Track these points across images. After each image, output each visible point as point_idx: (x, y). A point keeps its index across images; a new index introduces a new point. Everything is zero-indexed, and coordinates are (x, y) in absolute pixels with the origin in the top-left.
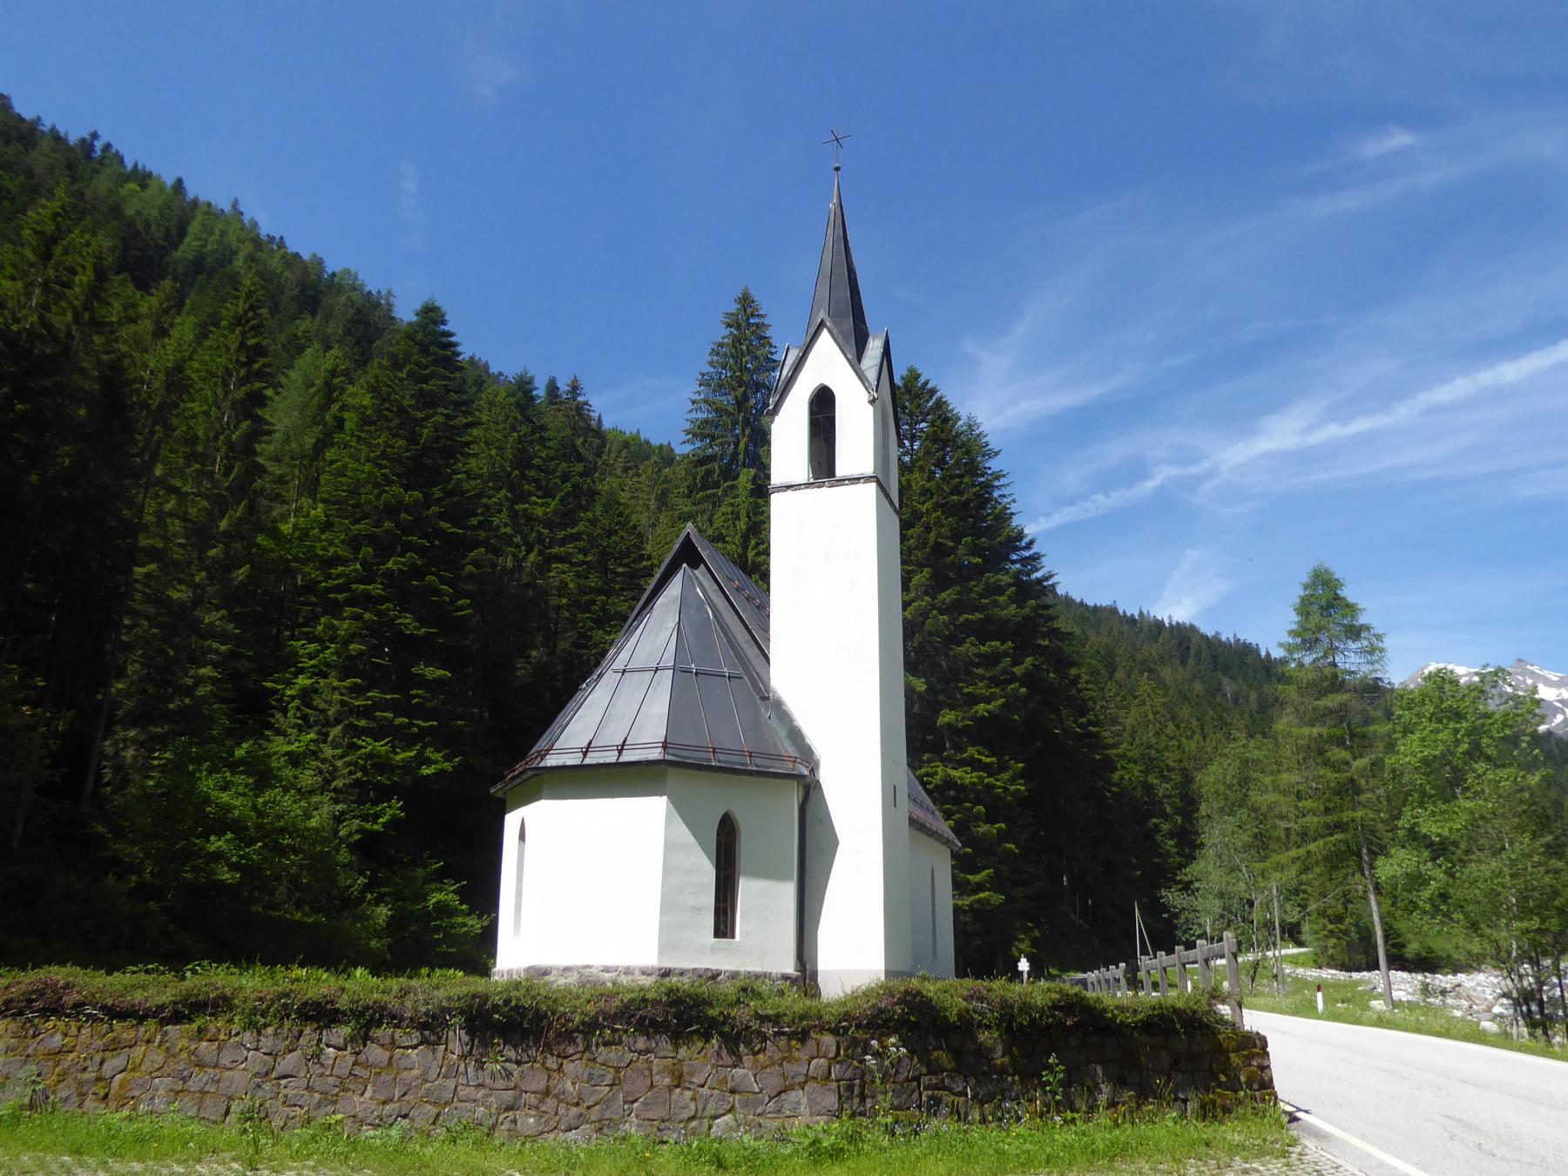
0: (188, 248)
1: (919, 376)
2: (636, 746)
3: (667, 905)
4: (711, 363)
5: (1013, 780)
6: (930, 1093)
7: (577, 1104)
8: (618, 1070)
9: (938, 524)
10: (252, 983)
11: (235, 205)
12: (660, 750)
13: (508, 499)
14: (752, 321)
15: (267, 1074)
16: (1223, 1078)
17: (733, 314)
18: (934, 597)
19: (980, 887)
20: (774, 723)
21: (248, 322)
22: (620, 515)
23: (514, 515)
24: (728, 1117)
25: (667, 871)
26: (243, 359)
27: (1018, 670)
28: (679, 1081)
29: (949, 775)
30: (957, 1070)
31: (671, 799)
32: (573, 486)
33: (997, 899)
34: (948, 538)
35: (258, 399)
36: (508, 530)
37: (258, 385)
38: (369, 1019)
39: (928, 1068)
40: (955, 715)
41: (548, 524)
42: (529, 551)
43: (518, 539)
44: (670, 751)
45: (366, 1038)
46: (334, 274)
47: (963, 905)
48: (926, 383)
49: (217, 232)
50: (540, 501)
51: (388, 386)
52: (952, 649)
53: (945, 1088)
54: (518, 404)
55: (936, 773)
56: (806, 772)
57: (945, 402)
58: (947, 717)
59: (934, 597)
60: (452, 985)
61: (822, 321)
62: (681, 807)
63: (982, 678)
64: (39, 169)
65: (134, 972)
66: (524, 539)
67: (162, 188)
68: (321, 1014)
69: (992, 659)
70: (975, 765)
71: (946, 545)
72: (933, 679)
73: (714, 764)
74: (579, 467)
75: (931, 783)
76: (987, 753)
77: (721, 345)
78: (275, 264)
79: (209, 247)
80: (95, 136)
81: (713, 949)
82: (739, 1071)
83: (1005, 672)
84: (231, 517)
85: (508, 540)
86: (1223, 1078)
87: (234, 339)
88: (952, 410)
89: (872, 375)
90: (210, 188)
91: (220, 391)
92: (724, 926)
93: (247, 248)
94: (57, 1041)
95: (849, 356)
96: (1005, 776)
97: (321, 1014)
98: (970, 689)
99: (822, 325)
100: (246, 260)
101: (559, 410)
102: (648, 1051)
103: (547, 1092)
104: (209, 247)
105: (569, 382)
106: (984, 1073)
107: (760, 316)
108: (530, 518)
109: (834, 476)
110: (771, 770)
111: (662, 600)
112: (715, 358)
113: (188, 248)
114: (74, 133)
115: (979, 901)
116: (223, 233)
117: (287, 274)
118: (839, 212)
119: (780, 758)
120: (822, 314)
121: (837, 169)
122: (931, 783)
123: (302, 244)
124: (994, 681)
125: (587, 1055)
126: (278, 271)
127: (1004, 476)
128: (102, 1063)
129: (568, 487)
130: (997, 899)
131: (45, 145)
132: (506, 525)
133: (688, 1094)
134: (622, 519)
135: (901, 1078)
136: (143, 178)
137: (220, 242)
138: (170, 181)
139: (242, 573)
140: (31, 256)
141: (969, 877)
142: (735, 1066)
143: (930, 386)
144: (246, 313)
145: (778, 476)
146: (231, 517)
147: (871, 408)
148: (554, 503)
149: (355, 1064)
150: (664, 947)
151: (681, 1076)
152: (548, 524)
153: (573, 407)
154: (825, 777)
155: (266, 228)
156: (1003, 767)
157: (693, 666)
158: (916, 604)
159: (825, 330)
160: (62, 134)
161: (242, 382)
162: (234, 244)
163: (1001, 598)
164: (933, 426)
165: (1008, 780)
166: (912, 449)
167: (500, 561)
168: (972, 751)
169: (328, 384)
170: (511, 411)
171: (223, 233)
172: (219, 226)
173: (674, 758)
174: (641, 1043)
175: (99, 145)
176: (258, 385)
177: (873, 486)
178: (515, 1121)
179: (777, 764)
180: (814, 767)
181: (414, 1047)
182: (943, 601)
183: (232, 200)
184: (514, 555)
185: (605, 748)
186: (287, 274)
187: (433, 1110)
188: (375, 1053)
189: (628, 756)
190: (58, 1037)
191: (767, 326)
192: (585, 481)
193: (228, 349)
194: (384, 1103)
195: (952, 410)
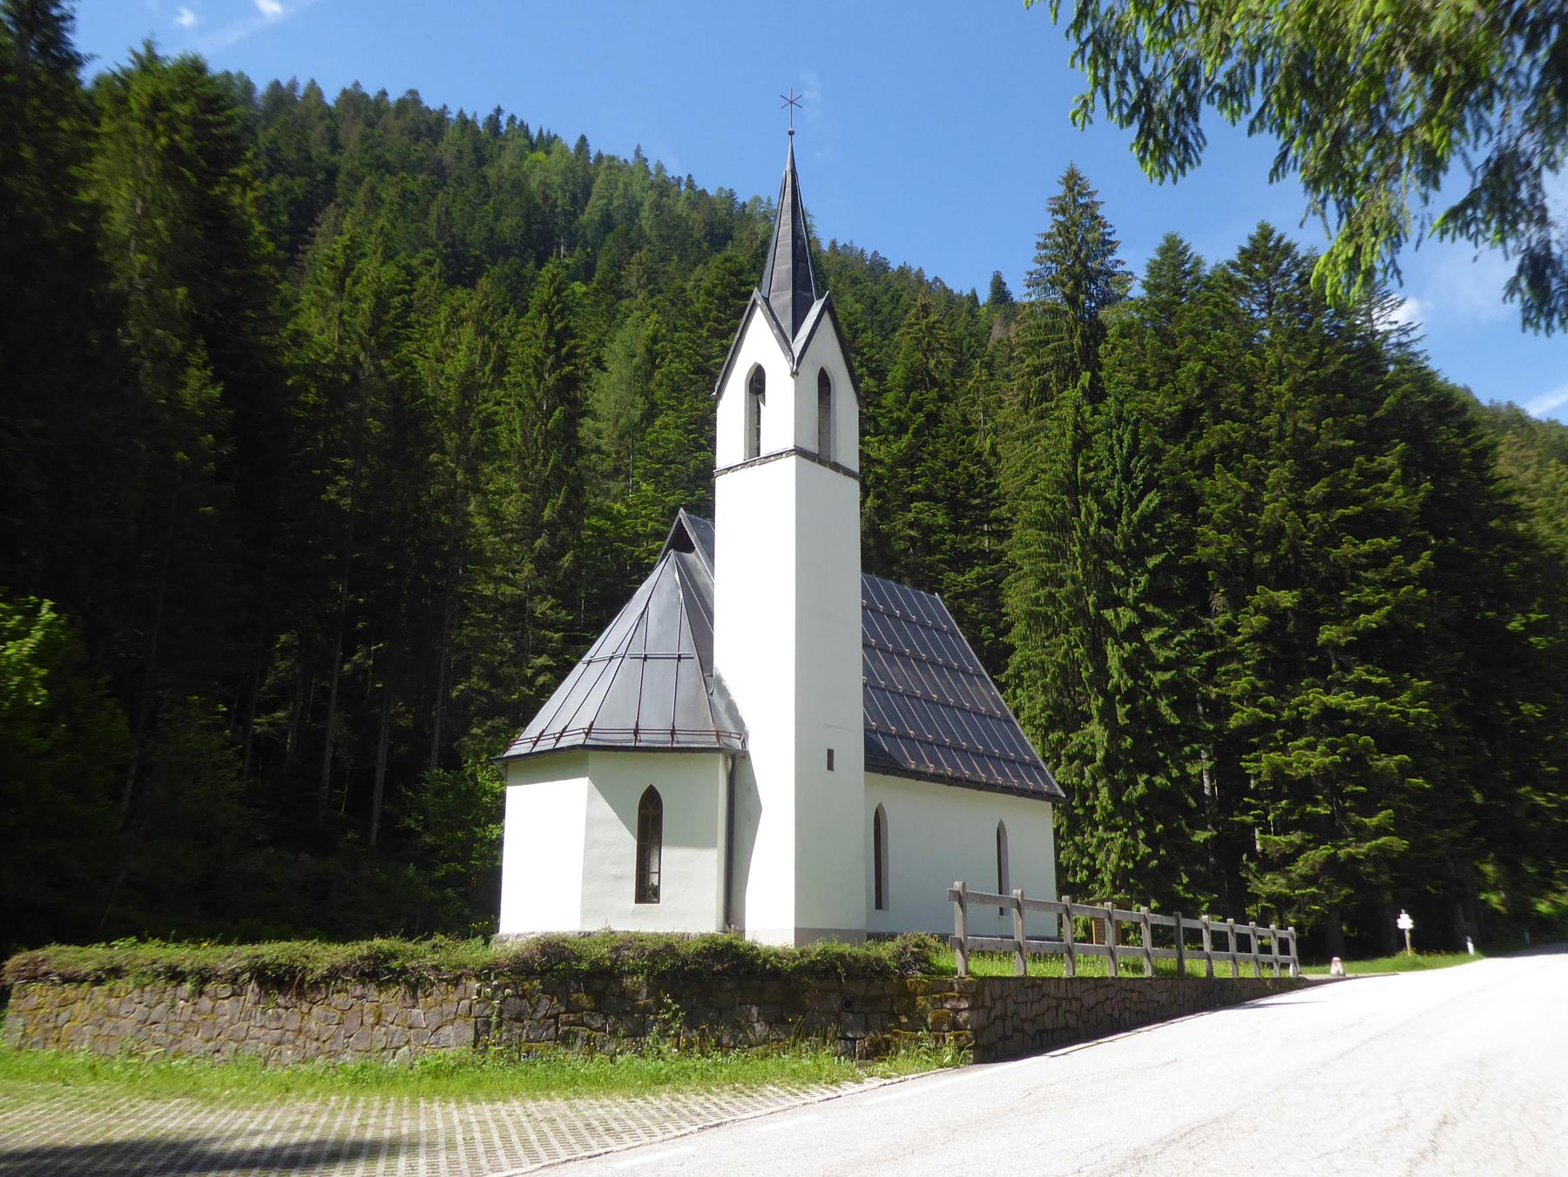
0: (591, 212)
1: (1272, 232)
3: (589, 874)
4: (1038, 260)
5: (1413, 702)
6: (566, 1028)
7: (317, 1039)
8: (343, 1011)
10: (155, 952)
11: (638, 152)
14: (1082, 201)
15: (145, 1021)
16: (904, 1020)
17: (1059, 198)
18: (1300, 490)
19: (1380, 831)
21: (554, 306)
24: (406, 1048)
25: (590, 844)
26: (552, 346)
27: (1414, 569)
28: (378, 1021)
30: (597, 1010)
33: (1399, 844)
35: (570, 383)
37: (568, 369)
38: (204, 977)
39: (567, 1007)
45: (201, 993)
46: (744, 205)
47: (1358, 853)
48: (1280, 239)
49: (621, 185)
51: (690, 348)
53: (583, 1025)
56: (738, 744)
58: (1327, 634)
60: (471, 952)
62: (600, 784)
63: (1370, 583)
64: (448, 159)
65: (121, 947)
67: (564, 150)
68: (175, 975)
69: (1379, 559)
70: (1362, 688)
74: (934, 393)
76: (1380, 671)
77: (1048, 236)
78: (680, 208)
79: (616, 203)
80: (499, 111)
81: (634, 913)
82: (416, 1011)
83: (1397, 572)
84: (554, 505)
86: (904, 1020)
87: (542, 325)
89: (797, 346)
90: (613, 143)
91: (533, 381)
92: (646, 892)
93: (651, 196)
94: (35, 1000)
96: (1405, 697)
97: (175, 975)
98: (1355, 597)
100: (651, 209)
102: (363, 997)
103: (300, 1031)
104: (616, 203)
106: (626, 1013)
107: (1090, 194)
112: (1043, 252)
113: (591, 212)
114: (480, 113)
115: (1378, 848)
116: (627, 186)
117: (694, 215)
122: (1308, 713)
123: (710, 184)
124: (1388, 585)
125: (326, 1002)
126: (684, 215)
127: (1413, 329)
128: (57, 1016)
129: (920, 417)
130: (1399, 844)
131: (452, 133)
133: (383, 1029)
134: (964, 447)
135: (539, 1015)
136: (546, 143)
137: (625, 196)
138: (571, 143)
139: (567, 560)
140: (329, 292)
141: (1366, 820)
142: (414, 1007)
144: (550, 298)
145: (721, 463)
146: (554, 505)
147: (792, 381)
149: (193, 1012)
150: (586, 913)
151: (380, 1016)
154: (753, 748)
155: (674, 170)
156: (1402, 687)
160: (469, 117)
161: (554, 368)
162: (639, 194)
163: (1385, 485)
165: (1409, 702)
168: (1359, 672)
169: (649, 351)
171: (627, 186)
172: (623, 179)
173: (594, 743)
174: (359, 991)
175: (503, 119)
176: (568, 369)
177: (792, 461)
178: (280, 1053)
180: (743, 735)
181: (228, 998)
182: (1314, 497)
183: (634, 148)
185: (575, 733)
186: (694, 215)
187: (235, 1045)
188: (205, 1003)
189: (564, 743)
190: (36, 997)
193: (537, 337)
194: (208, 1041)
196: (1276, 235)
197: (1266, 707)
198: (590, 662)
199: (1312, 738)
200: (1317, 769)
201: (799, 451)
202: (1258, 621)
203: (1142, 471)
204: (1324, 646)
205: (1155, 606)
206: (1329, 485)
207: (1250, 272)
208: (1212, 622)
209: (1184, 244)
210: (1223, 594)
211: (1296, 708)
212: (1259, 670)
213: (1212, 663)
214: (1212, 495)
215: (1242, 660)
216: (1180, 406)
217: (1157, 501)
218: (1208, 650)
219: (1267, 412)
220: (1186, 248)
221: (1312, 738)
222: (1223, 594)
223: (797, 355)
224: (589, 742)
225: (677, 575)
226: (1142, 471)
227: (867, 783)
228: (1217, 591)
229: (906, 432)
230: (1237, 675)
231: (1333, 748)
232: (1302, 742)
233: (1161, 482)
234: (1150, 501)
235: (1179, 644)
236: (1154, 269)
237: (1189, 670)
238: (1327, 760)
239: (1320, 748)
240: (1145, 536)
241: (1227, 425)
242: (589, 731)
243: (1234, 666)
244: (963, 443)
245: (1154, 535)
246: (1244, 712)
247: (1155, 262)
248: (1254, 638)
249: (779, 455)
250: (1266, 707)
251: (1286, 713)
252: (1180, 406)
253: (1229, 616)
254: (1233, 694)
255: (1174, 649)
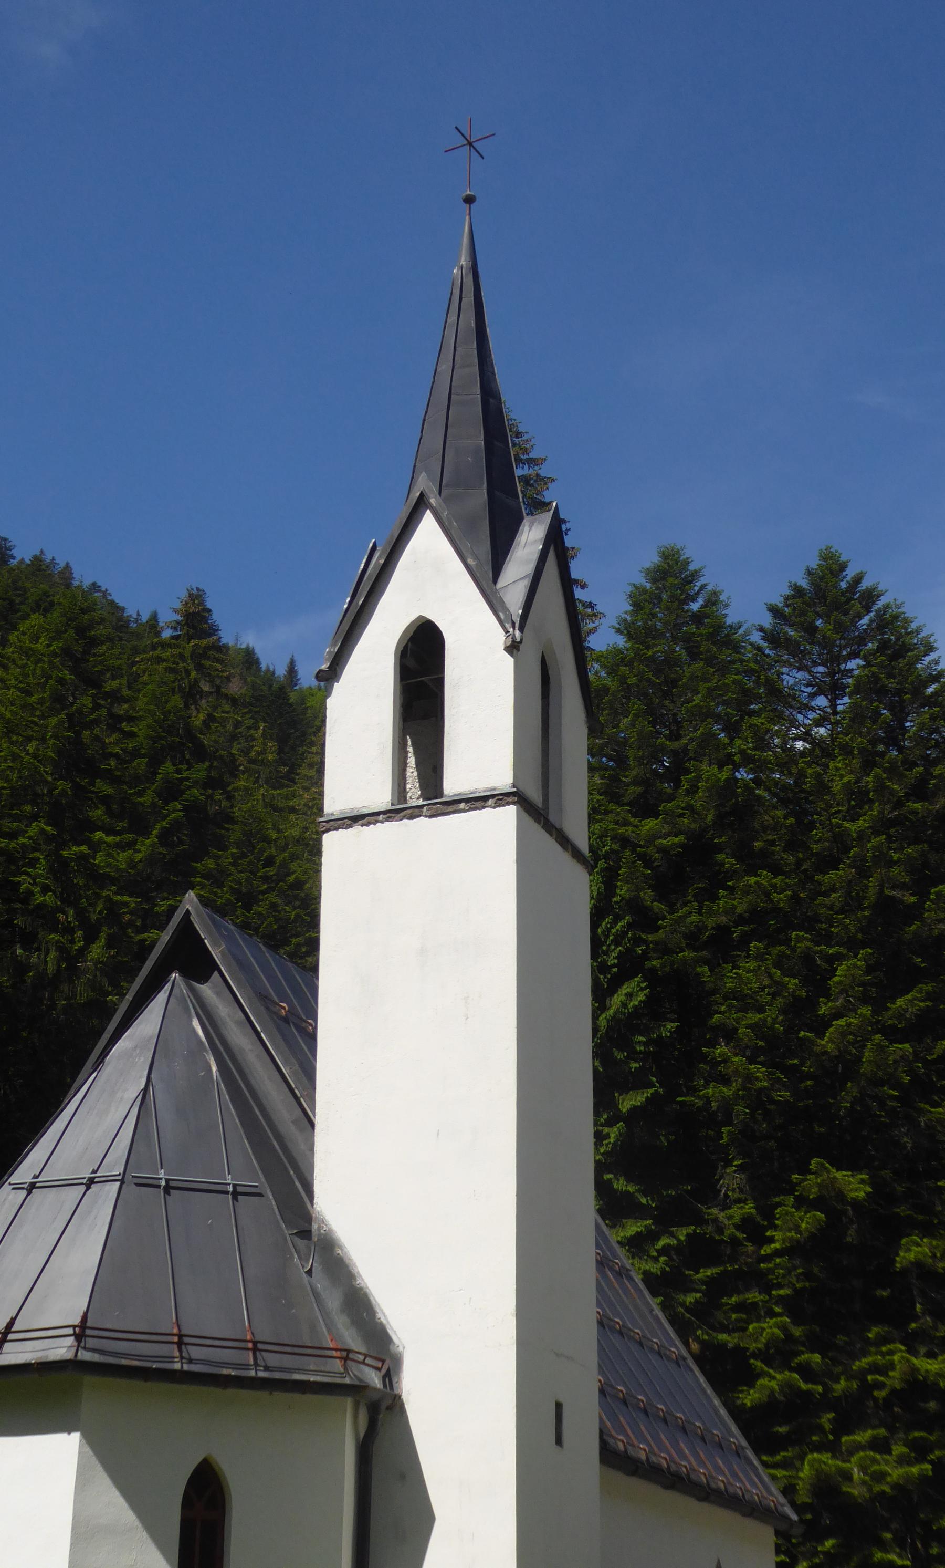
1: (843, 567)
2: (31, 1335)
9: (883, 860)
12: (70, 1341)
13: (49, 839)
18: (879, 1007)
20: (320, 1281)
22: (269, 862)
23: (60, 868)
29: (914, 1370)
31: (89, 1438)
32: (185, 809)
34: (903, 887)
36: (49, 898)
40: (932, 1248)
41: (129, 885)
42: (90, 939)
43: (69, 916)
44: (90, 1342)
48: (858, 580)
50: (110, 839)
52: (921, 1112)
54: (67, 652)
55: (892, 1366)
56: (375, 1379)
57: (896, 617)
59: (879, 1007)
61: (422, 495)
66: (81, 915)
71: (901, 901)
72: (887, 1174)
73: (177, 1366)
74: (199, 772)
75: (880, 1386)
85: (45, 916)
88: (918, 631)
89: (514, 598)
95: (470, 561)
99: (420, 505)
101: (159, 660)
105: (178, 605)
107: (533, 462)
108: (98, 878)
109: (441, 794)
110: (297, 1377)
111: (122, 1045)
118: (469, 282)
119: (319, 1352)
120: (424, 483)
121: (469, 200)
132: (45, 889)
134: (272, 871)
143: (865, 584)
147: (509, 661)
148: (146, 846)
152: (129, 885)
153: (187, 654)
157: (162, 1174)
158: (842, 1022)
159: (428, 512)
164: (869, 664)
166: (835, 713)
167: (34, 959)
170: (53, 666)
173: (96, 1358)
177: (510, 812)
179: (312, 1364)
182: (900, 1016)
184: (61, 948)
185: (49, 1333)
191: (545, 481)
192: (210, 797)
195: (918, 631)
196: (850, 573)
197: (806, 1372)
198: (32, 1187)
199: (882, 1432)
200: (895, 1486)
201: (516, 797)
202: (809, 1221)
203: (617, 942)
204: (904, 1272)
205: (629, 1180)
206: (929, 997)
207: (811, 630)
208: (722, 1216)
209: (692, 567)
210: (741, 1168)
211: (863, 1373)
212: (793, 1306)
213: (716, 1288)
214: (733, 995)
215: (767, 1288)
216: (680, 839)
217: (641, 997)
218: (707, 1265)
219: (833, 863)
220: (695, 575)
221: (882, 1432)
222: (741, 1168)
223: (517, 611)
224: (85, 1356)
225: (196, 1024)
226: (617, 942)
227: (600, 1467)
228: (728, 1163)
229: (146, 833)
230: (750, 1311)
231: (920, 1451)
232: (862, 1437)
233: (648, 964)
234: (630, 996)
235: (664, 1251)
236: (640, 600)
237: (681, 1298)
238: (915, 1470)
239: (899, 1449)
240: (619, 1056)
241: (764, 878)
242: (81, 1332)
243: (754, 1296)
244: (269, 862)
245: (633, 1055)
246: (774, 1378)
247: (645, 591)
248: (790, 1251)
249: (477, 801)
250: (806, 1372)
251: (840, 1386)
252: (680, 839)
253: (749, 1208)
254: (753, 1346)
255: (656, 1259)
